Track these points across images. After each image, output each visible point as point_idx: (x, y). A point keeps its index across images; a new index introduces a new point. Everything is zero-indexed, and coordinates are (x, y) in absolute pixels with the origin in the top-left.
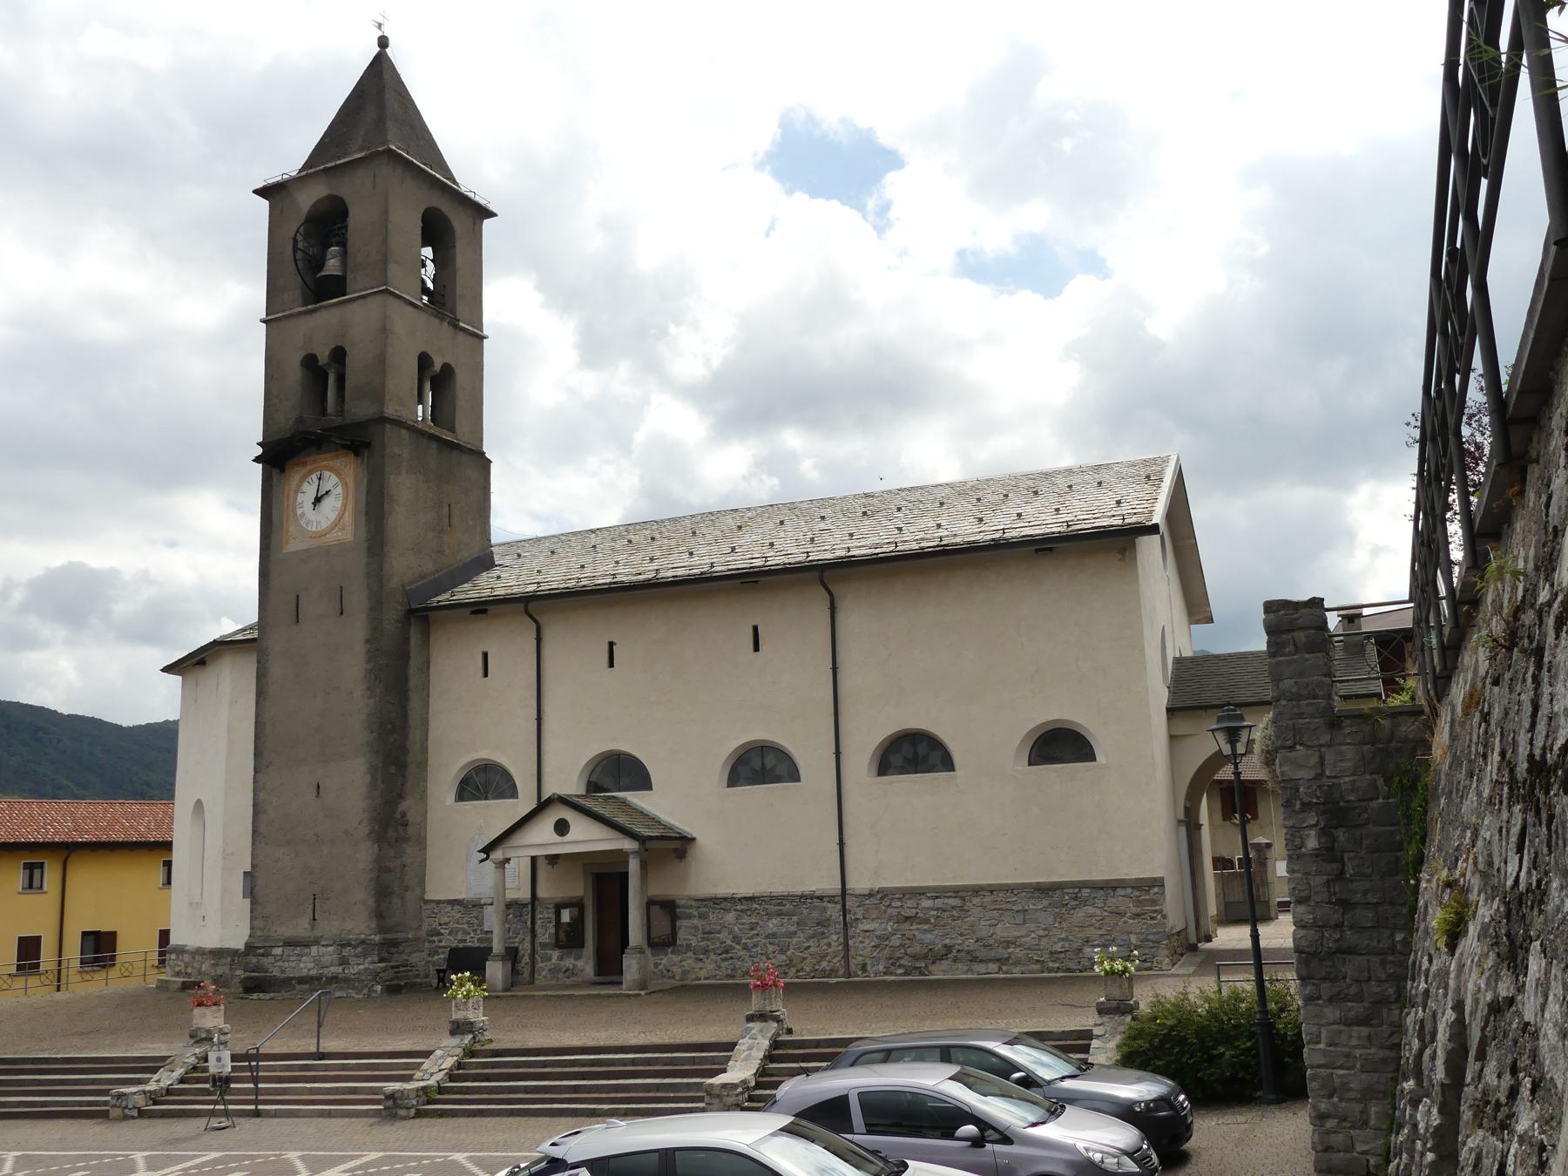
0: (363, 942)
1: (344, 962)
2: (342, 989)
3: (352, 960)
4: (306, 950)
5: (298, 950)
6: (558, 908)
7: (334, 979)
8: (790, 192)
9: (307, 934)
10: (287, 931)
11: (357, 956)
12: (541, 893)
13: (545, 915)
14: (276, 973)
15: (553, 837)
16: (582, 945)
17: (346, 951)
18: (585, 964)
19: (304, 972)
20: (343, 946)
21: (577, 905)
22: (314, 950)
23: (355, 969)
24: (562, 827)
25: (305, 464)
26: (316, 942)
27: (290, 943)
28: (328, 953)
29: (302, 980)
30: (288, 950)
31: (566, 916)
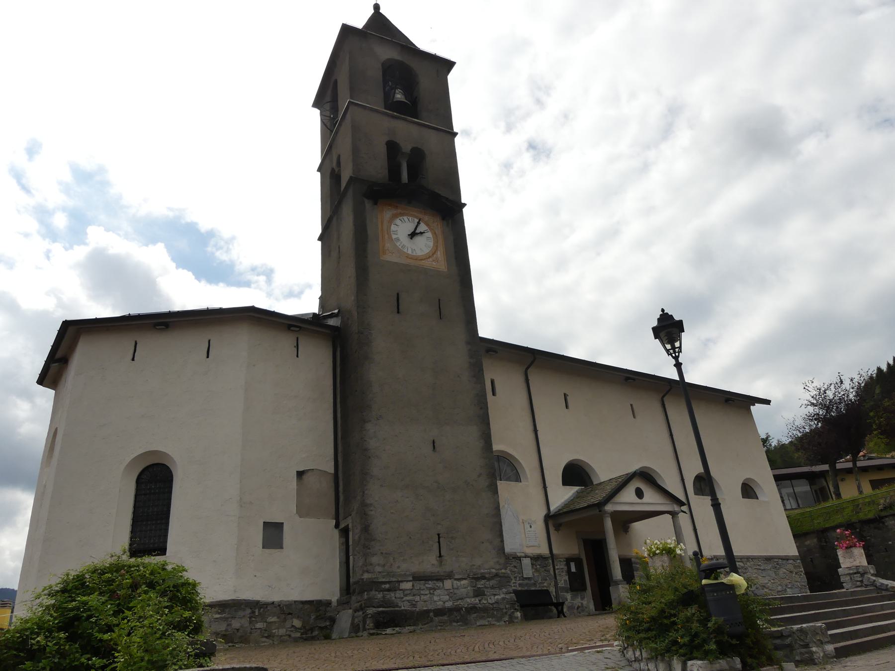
0: (497, 575)
1: (479, 593)
2: (482, 618)
3: (488, 592)
4: (440, 584)
5: (430, 584)
6: (568, 561)
7: (473, 609)
8: (465, 205)
9: (436, 570)
10: (415, 567)
11: (492, 588)
12: (555, 551)
13: (561, 566)
14: (405, 606)
15: (635, 499)
16: (585, 589)
17: (481, 584)
18: (587, 601)
19: (440, 605)
20: (477, 579)
21: (578, 561)
22: (448, 584)
23: (492, 600)
24: (639, 493)
25: (396, 207)
26: (450, 576)
27: (418, 578)
28: (464, 587)
29: (439, 612)
30: (419, 585)
31: (573, 565)
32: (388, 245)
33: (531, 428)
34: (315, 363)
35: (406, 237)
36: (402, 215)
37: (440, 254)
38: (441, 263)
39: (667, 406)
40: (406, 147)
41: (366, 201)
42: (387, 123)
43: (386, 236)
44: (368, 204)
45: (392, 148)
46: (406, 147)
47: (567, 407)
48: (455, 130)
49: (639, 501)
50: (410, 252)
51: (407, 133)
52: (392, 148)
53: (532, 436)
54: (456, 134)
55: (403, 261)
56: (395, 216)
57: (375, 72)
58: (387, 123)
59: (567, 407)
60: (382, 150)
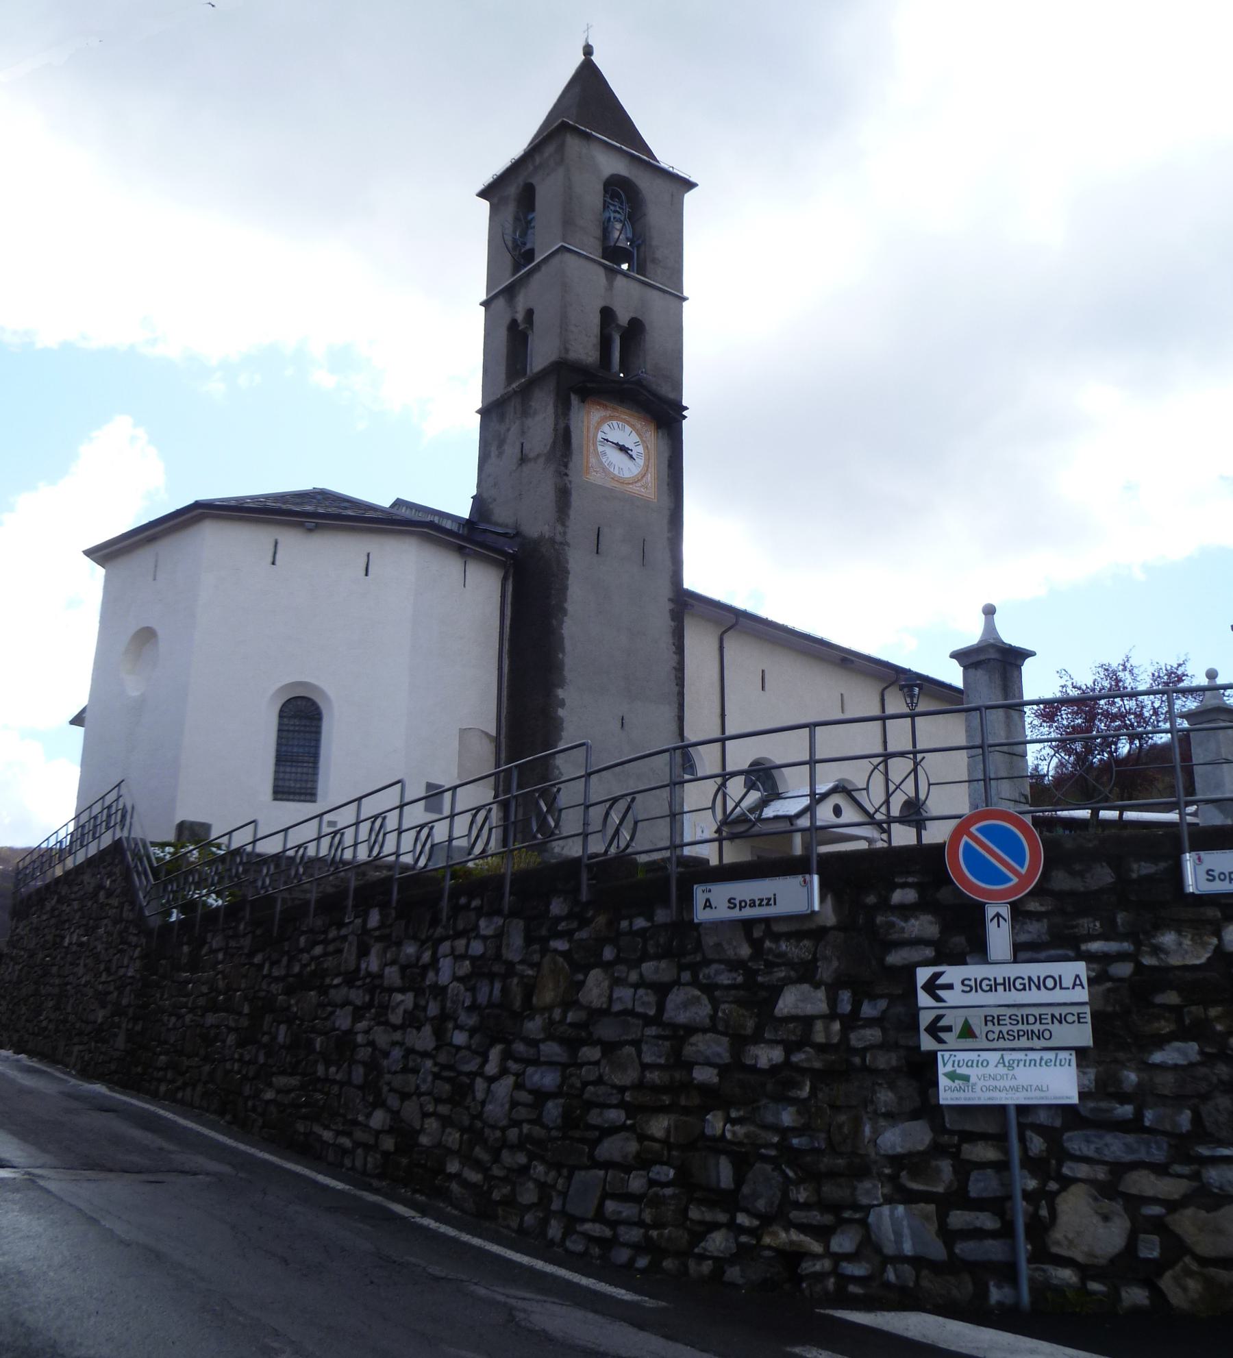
24: (837, 811)
25: (606, 407)
32: (593, 460)
33: (718, 711)
34: (472, 600)
35: (614, 447)
36: (611, 418)
37: (650, 477)
38: (650, 489)
39: (725, 645)
40: (623, 318)
41: (573, 397)
42: (584, 263)
43: (592, 448)
44: (574, 400)
45: (607, 314)
46: (623, 318)
47: (367, 575)
48: (686, 294)
49: (308, 809)
50: (616, 472)
51: (627, 297)
52: (607, 314)
53: (718, 721)
54: (685, 299)
55: (610, 484)
56: (603, 420)
57: (592, 196)
58: (584, 263)
59: (367, 575)
60: (596, 319)
